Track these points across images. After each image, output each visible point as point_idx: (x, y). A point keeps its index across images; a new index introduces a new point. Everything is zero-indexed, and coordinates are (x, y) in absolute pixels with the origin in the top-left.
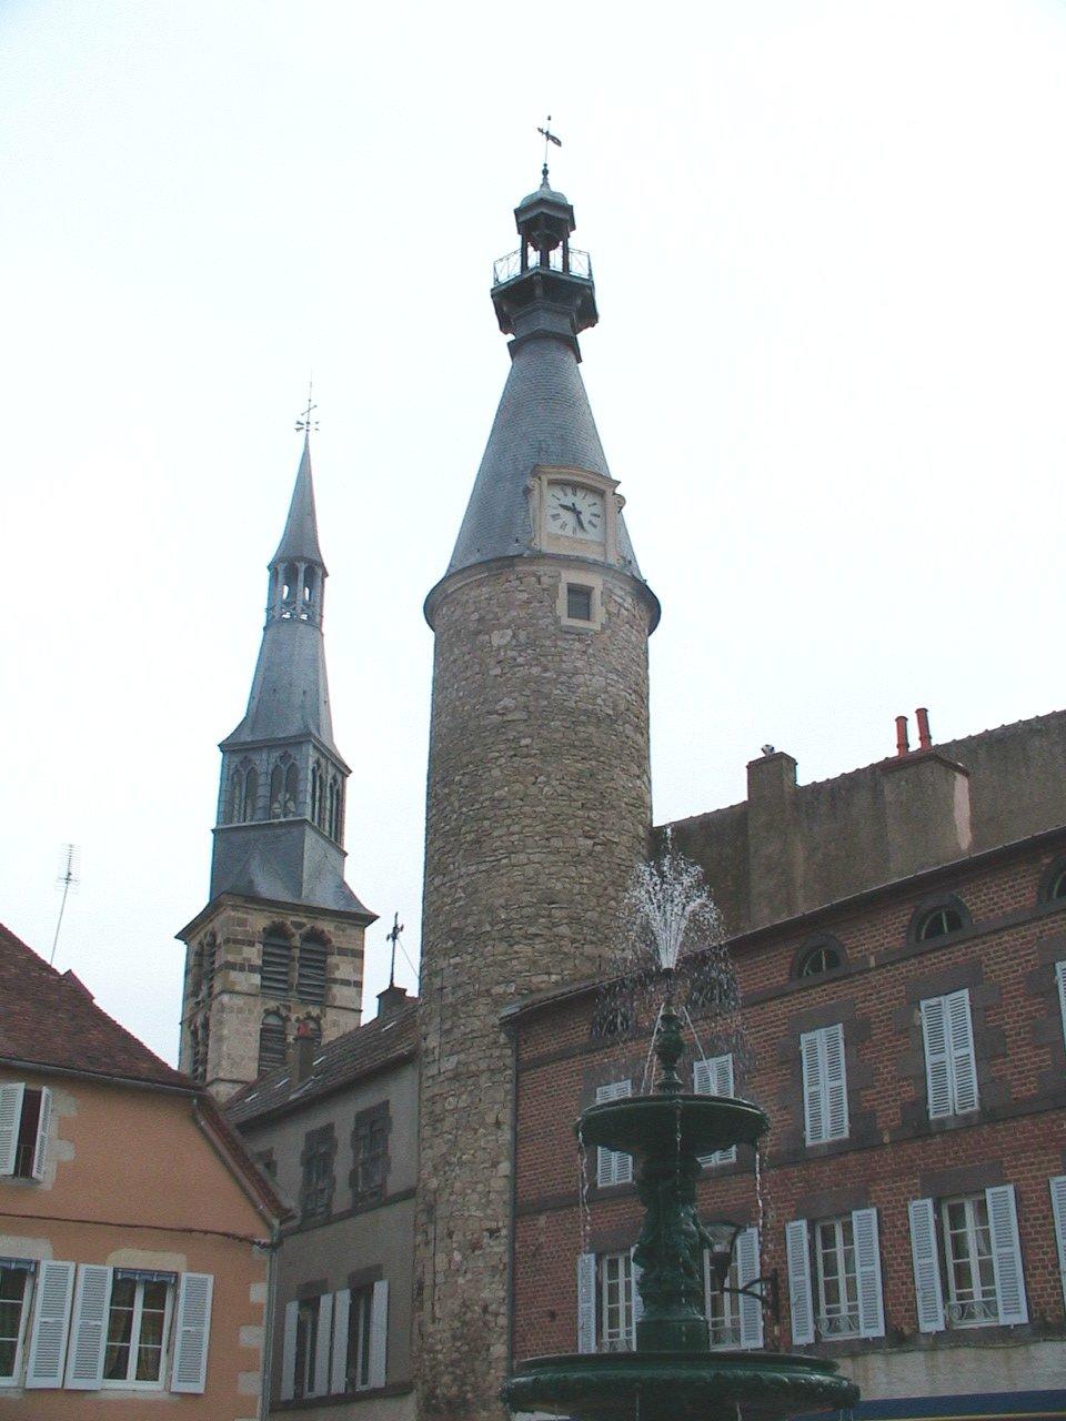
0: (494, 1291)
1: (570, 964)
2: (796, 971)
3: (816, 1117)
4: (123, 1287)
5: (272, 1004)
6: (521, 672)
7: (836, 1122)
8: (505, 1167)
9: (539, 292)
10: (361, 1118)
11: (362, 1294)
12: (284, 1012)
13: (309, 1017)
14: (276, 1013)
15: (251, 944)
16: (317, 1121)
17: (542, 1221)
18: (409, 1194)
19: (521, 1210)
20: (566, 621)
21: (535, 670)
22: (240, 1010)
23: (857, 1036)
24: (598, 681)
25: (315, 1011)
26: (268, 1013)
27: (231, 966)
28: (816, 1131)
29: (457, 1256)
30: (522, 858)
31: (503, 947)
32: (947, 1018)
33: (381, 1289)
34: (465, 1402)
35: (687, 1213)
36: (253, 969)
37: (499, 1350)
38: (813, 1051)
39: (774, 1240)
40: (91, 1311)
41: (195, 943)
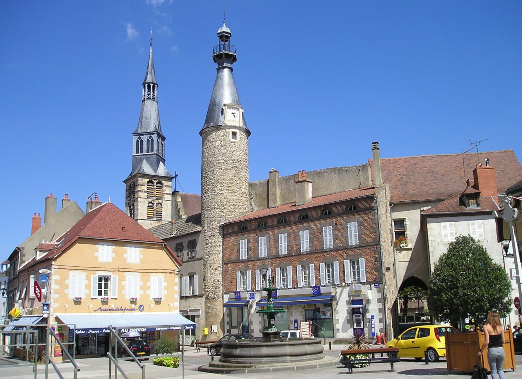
0: (220, 278)
1: (233, 214)
2: (278, 223)
3: (281, 249)
4: (100, 280)
5: (150, 200)
6: (223, 151)
7: (307, 248)
8: (221, 254)
9: (224, 57)
10: (189, 242)
11: (191, 277)
12: (153, 202)
13: (159, 203)
14: (151, 202)
15: (144, 185)
16: (179, 241)
17: (229, 265)
18: (201, 259)
19: (225, 263)
20: (232, 140)
21: (226, 151)
22: (143, 202)
23: (289, 236)
24: (238, 153)
25: (160, 201)
26: (150, 203)
27: (140, 191)
28: (326, 245)
29: (212, 271)
30: (223, 192)
31: (220, 210)
32: (305, 235)
33: (196, 277)
34: (215, 298)
35: (472, 318)
36: (145, 192)
37: (221, 288)
38: (281, 238)
39: (273, 271)
40: (94, 284)
41: (128, 184)
